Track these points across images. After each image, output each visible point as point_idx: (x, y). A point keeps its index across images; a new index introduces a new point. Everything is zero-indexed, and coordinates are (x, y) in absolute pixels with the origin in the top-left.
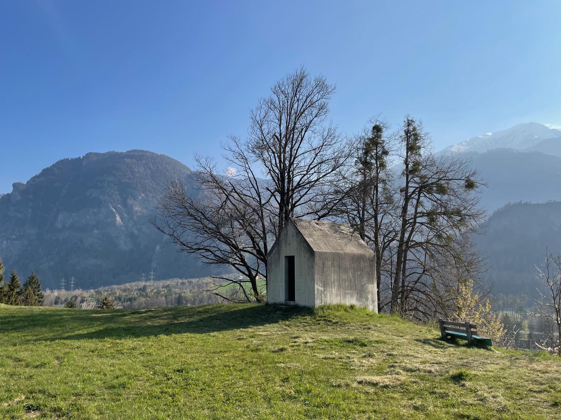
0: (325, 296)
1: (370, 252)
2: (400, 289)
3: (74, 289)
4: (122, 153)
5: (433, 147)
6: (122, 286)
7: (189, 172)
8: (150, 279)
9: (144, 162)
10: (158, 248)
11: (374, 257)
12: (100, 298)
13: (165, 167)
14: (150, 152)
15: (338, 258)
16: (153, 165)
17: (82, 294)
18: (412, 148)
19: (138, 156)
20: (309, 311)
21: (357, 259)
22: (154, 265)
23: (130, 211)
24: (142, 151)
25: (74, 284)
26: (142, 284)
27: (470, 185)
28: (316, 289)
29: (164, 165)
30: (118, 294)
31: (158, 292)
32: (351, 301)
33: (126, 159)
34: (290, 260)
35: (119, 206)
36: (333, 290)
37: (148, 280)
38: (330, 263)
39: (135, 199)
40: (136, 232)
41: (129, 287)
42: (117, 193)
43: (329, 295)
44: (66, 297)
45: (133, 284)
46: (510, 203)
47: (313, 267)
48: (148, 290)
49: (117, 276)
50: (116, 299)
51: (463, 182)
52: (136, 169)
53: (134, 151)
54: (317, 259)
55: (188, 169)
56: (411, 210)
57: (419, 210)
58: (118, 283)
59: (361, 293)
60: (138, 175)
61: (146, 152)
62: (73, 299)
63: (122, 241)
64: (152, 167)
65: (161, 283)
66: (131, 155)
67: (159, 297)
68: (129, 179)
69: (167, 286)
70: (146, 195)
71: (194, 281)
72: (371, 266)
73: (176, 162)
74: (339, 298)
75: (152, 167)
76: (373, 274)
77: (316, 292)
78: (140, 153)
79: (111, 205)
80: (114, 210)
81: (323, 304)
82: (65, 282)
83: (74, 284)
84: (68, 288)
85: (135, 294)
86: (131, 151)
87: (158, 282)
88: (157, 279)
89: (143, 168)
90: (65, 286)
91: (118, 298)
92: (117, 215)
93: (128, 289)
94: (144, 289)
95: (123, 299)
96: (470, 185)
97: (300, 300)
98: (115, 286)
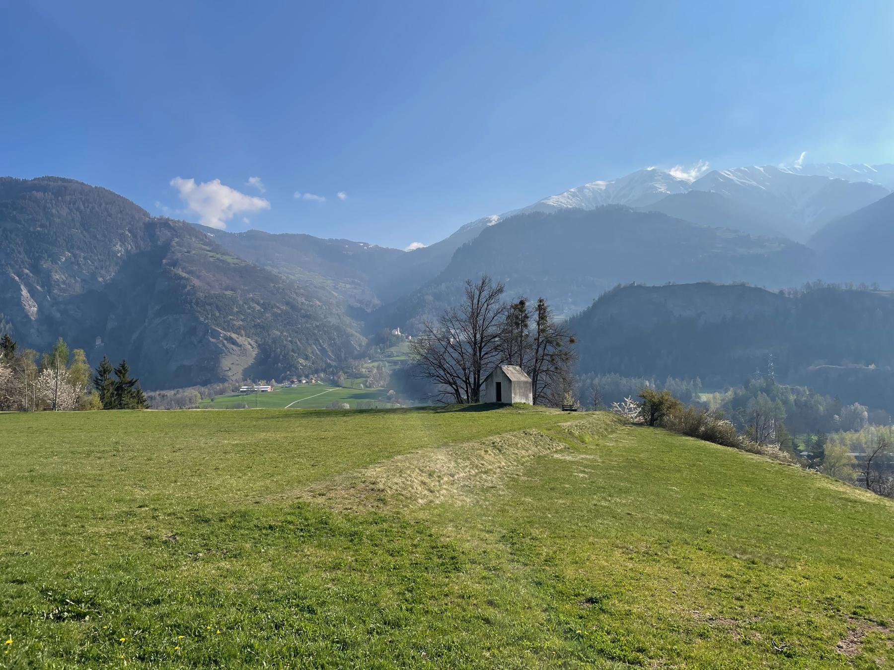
1: (530, 380)
4: (25, 181)
5: (557, 318)
7: (147, 219)
9: (68, 198)
10: (98, 342)
13: (106, 209)
14: (77, 182)
15: (519, 382)
16: (84, 204)
18: (542, 317)
19: (59, 189)
20: (510, 405)
21: (526, 382)
23: (47, 281)
24: (63, 180)
27: (572, 341)
29: (104, 205)
32: (523, 401)
33: (34, 192)
34: (499, 385)
35: (27, 271)
39: (55, 261)
40: (58, 315)
42: (21, 250)
43: (517, 399)
46: (620, 285)
51: (568, 339)
52: (54, 211)
53: (49, 179)
55: (146, 214)
56: (541, 351)
57: (546, 352)
60: (57, 220)
61: (71, 181)
63: (33, 331)
64: (82, 207)
66: (41, 185)
68: (42, 226)
70: (75, 256)
71: (170, 393)
73: (125, 201)
75: (82, 207)
78: (60, 183)
79: (10, 270)
80: (17, 278)
86: (43, 179)
89: (67, 210)
92: (22, 287)
96: (572, 341)
97: (504, 400)
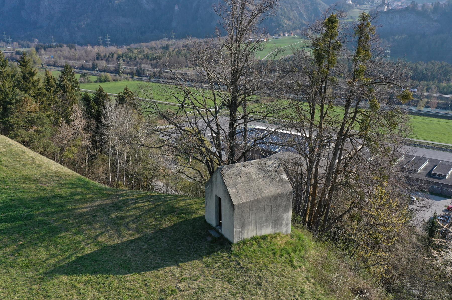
0: (243, 234)
2: (335, 169)
3: (111, 45)
6: (149, 44)
8: (172, 39)
10: (176, 8)
11: (291, 192)
12: (131, 55)
17: (117, 51)
22: (174, 24)
25: (110, 41)
26: (165, 42)
28: (234, 231)
30: (146, 53)
31: (179, 52)
36: (250, 227)
37: (170, 38)
38: (248, 209)
41: (155, 46)
44: (104, 54)
45: (158, 42)
47: (232, 215)
48: (171, 49)
49: (142, 36)
50: (145, 58)
54: (236, 210)
58: (146, 41)
59: (276, 222)
62: (111, 56)
65: (181, 43)
67: (180, 57)
69: (185, 46)
72: (288, 200)
74: (255, 231)
76: (289, 205)
77: (234, 233)
81: (240, 239)
82: (102, 39)
83: (110, 41)
84: (105, 45)
85: (159, 53)
87: (178, 41)
88: (178, 37)
90: (103, 42)
91: (147, 56)
93: (154, 48)
94: (166, 48)
95: (150, 58)
98: (143, 44)
